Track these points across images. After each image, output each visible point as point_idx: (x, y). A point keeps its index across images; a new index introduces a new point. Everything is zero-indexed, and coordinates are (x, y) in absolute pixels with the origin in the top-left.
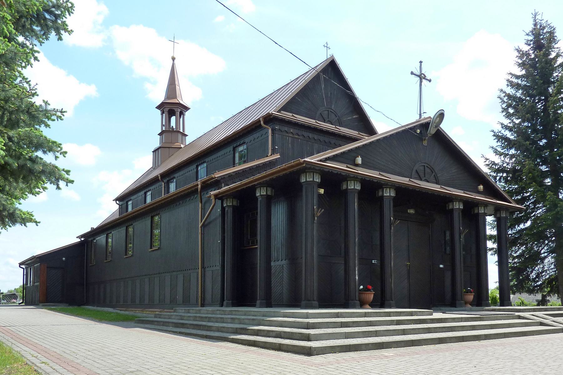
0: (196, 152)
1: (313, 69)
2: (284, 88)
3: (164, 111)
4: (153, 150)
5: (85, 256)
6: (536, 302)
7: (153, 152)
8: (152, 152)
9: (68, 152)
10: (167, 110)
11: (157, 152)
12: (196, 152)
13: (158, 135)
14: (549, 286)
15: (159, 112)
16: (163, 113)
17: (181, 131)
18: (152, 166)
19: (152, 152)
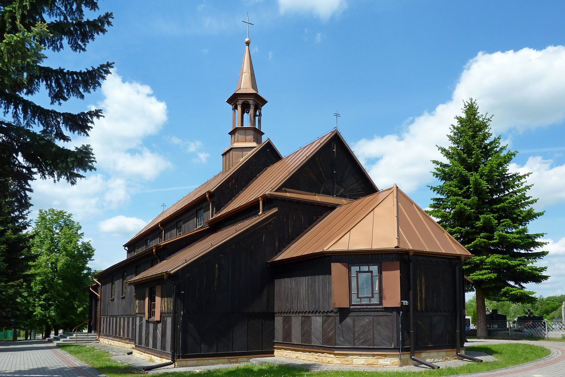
0: (227, 211)
1: (337, 116)
2: (291, 156)
3: (237, 104)
4: (222, 153)
5: (369, 346)
6: (51, 336)
7: (223, 155)
8: (222, 155)
9: (93, 42)
10: (240, 102)
11: (228, 155)
12: (227, 211)
13: (228, 134)
14: (533, 302)
15: (230, 107)
16: (235, 108)
17: (257, 127)
18: (262, 108)
19: (222, 155)
